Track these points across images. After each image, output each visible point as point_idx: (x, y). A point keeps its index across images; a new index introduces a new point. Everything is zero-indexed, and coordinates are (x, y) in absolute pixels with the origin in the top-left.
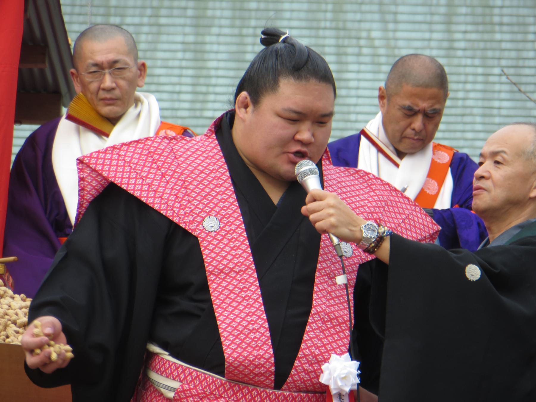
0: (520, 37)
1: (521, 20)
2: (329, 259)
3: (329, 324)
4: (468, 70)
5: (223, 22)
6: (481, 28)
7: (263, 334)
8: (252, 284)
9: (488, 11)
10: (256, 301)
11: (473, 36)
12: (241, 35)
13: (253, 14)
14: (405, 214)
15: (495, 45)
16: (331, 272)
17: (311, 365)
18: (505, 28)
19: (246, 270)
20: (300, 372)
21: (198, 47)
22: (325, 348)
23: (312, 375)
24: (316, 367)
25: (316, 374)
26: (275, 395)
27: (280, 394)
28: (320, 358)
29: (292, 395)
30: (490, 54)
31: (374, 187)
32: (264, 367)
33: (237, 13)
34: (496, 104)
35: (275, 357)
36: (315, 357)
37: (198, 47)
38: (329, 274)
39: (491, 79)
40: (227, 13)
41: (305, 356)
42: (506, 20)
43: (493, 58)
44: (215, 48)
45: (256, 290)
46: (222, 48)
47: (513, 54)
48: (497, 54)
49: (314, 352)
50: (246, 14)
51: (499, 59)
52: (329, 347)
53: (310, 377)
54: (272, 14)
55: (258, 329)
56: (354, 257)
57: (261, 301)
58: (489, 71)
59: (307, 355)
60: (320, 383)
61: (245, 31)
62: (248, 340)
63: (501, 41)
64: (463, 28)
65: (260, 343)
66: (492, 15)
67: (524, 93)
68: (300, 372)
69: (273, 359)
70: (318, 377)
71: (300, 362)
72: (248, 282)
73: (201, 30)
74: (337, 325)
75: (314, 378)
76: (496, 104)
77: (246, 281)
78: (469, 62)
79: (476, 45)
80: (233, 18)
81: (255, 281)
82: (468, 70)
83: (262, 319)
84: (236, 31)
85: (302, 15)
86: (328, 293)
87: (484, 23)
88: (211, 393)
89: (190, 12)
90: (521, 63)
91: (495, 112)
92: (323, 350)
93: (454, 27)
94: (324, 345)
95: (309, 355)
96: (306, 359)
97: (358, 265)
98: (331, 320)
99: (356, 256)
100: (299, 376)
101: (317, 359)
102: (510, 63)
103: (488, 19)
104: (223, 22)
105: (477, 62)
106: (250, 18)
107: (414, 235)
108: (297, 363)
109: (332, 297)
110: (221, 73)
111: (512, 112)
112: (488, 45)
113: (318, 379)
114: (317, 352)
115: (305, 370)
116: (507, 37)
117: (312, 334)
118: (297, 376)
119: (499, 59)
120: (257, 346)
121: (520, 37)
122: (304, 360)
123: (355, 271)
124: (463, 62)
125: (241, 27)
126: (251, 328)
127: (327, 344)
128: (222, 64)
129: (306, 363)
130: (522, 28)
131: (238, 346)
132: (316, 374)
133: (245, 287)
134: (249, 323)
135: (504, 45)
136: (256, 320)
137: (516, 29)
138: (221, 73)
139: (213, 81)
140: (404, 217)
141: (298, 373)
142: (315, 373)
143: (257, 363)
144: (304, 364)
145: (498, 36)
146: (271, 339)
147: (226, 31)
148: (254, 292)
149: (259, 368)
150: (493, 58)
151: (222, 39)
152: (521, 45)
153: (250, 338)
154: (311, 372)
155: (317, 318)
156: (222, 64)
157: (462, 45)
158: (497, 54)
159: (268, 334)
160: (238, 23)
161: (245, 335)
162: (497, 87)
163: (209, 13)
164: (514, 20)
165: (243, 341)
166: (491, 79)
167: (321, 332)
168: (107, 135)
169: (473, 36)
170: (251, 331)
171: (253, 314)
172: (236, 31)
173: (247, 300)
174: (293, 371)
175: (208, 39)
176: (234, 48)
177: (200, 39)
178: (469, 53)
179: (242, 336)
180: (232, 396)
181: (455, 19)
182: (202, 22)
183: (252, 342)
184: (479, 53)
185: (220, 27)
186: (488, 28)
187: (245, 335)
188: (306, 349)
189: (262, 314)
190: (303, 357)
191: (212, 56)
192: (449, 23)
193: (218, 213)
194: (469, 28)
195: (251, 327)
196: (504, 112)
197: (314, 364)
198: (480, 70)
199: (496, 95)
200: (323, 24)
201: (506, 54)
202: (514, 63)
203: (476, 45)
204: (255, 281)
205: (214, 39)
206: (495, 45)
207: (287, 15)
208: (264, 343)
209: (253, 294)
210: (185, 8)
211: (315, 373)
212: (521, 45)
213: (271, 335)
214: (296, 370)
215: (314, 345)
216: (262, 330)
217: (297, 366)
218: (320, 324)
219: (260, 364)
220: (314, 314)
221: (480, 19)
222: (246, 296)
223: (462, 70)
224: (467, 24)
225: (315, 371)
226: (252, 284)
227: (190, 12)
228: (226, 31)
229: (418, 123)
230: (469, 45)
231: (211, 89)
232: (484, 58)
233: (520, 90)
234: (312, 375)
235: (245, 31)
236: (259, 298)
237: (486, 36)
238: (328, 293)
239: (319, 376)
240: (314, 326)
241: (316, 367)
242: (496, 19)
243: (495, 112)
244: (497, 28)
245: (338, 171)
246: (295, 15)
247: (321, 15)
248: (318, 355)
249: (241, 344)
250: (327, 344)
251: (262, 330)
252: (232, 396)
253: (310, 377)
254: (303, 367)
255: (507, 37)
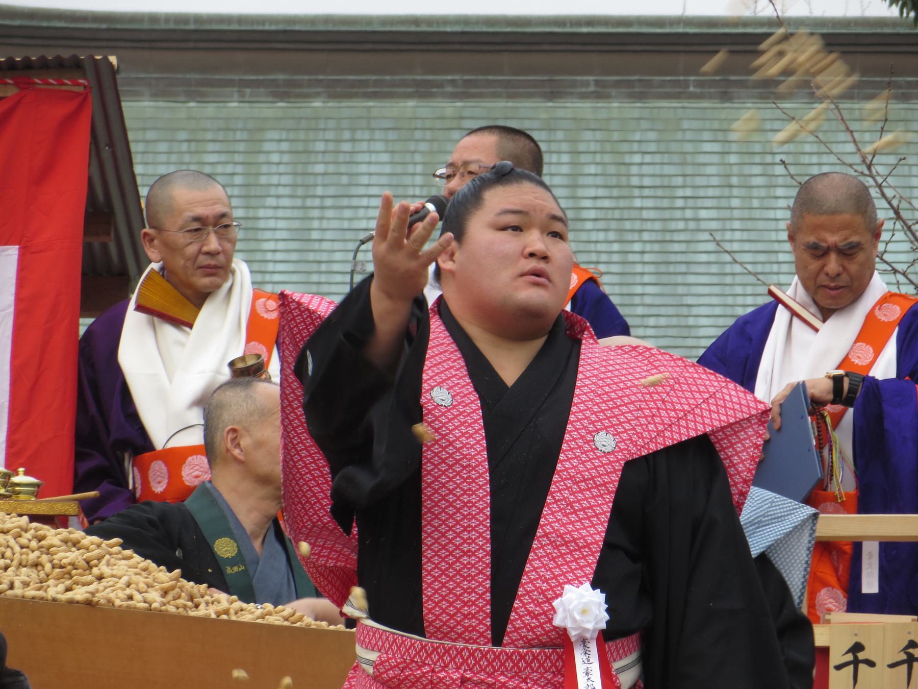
0: (665, 203)
1: (666, 181)
2: (577, 457)
3: (563, 550)
4: (600, 247)
5: (281, 191)
6: (615, 192)
7: (480, 560)
8: (481, 487)
9: (623, 169)
10: (481, 511)
11: (607, 203)
12: (304, 207)
13: (319, 180)
14: (708, 392)
15: (634, 214)
16: (577, 473)
17: (539, 605)
18: (646, 192)
19: (477, 466)
20: (523, 616)
21: (250, 224)
22: (557, 580)
23: (543, 619)
24: (546, 607)
25: (548, 618)
26: (494, 653)
27: (501, 652)
28: (550, 594)
29: (519, 653)
30: (628, 225)
31: (657, 364)
32: (476, 605)
33: (299, 180)
34: (639, 290)
35: (491, 593)
36: (543, 592)
37: (250, 224)
38: (574, 476)
39: (632, 258)
40: (286, 180)
41: (528, 593)
42: (647, 181)
43: (632, 231)
44: (272, 224)
45: (484, 496)
46: (281, 224)
47: (658, 226)
48: (637, 225)
49: (540, 587)
50: (310, 180)
51: (641, 231)
52: (561, 579)
53: (539, 622)
54: (345, 180)
55: (475, 551)
56: (618, 452)
57: (488, 513)
58: (627, 247)
59: (531, 592)
60: (555, 628)
61: (309, 202)
62: (458, 566)
63: (641, 209)
64: (592, 192)
65: (473, 572)
66: (629, 175)
67: (741, 264)
68: (523, 616)
69: (488, 594)
70: (550, 620)
71: (521, 601)
72: (476, 483)
73: (253, 202)
74: (575, 550)
75: (546, 623)
76: (639, 290)
77: (474, 481)
78: (601, 236)
79: (610, 214)
80: (294, 185)
81: (486, 484)
82: (600, 247)
83: (484, 538)
84: (299, 202)
85: (384, 180)
86: (568, 505)
87: (618, 186)
88: (412, 661)
89: (238, 180)
90: (668, 237)
91: (637, 300)
92: (553, 583)
93: (581, 192)
94: (555, 577)
95: (534, 591)
96: (530, 596)
97: (622, 462)
98: (566, 544)
99: (621, 450)
100: (522, 621)
101: (545, 596)
102: (654, 236)
103: (624, 180)
104: (281, 191)
105: (612, 236)
106: (316, 185)
107: (723, 418)
108: (517, 604)
109: (578, 510)
110: (279, 256)
111: (658, 301)
112: (626, 214)
113: (551, 624)
114: (545, 586)
115: (529, 613)
116: (649, 203)
117: (537, 564)
118: (519, 622)
119: (641, 231)
120: (469, 575)
121: (665, 203)
122: (526, 599)
123: (618, 470)
124: (594, 236)
125: (305, 197)
126: (465, 549)
127: (560, 575)
128: (281, 245)
129: (530, 603)
130: (667, 193)
131: (443, 572)
132: (548, 618)
133: (470, 489)
134: (465, 541)
135: (645, 214)
136: (476, 539)
137: (660, 192)
138: (279, 256)
139: (270, 267)
140: (706, 396)
141: (521, 617)
142: (546, 615)
143: (466, 599)
144: (527, 604)
145: (638, 203)
146: (491, 568)
147: (285, 202)
148: (481, 499)
149: (469, 607)
150: (632, 231)
151: (280, 213)
152: (667, 214)
153: (462, 564)
154: (540, 614)
155: (545, 541)
156: (281, 245)
157: (592, 214)
158: (637, 225)
159: (488, 560)
160: (300, 191)
161: (455, 557)
162: (639, 268)
163: (263, 180)
164: (658, 181)
165: (451, 566)
166: (632, 258)
167: (550, 560)
168: (191, 326)
169: (607, 203)
170: (465, 553)
171: (473, 529)
172: (299, 202)
173: (470, 508)
174: (513, 615)
175: (261, 213)
176: (296, 224)
177: (251, 213)
178: (601, 225)
179: (451, 559)
180: (438, 661)
181: (582, 181)
182: (253, 191)
183: (463, 568)
184: (613, 225)
185: (278, 197)
186: (625, 192)
187: (455, 557)
188: (529, 583)
189: (486, 531)
190: (525, 595)
191: (268, 235)
192: (575, 186)
193: (618, 434)
194: (601, 192)
195: (465, 547)
196: (648, 300)
197: (542, 603)
198: (616, 247)
199: (638, 279)
200: (410, 192)
201: (649, 225)
202: (659, 237)
203: (610, 214)
204: (486, 484)
205: (270, 213)
206: (634, 214)
207: (364, 180)
208: (481, 572)
209: (479, 501)
210: (233, 174)
211: (546, 615)
212: (667, 214)
213: (492, 562)
214: (517, 613)
215: (540, 577)
216: (481, 554)
217: (518, 608)
218: (549, 549)
219: (470, 601)
220: (540, 537)
221: (613, 181)
222: (469, 502)
223: (592, 247)
224: (597, 187)
225: (545, 613)
226: (481, 487)
227: (238, 180)
228: (285, 202)
229: (833, 264)
230: (600, 214)
231: (268, 278)
232: (621, 231)
233: (735, 261)
234: (543, 619)
235: (309, 202)
236: (486, 507)
237: (622, 203)
238: (568, 505)
239: (552, 619)
240: (541, 552)
241: (546, 607)
242: (635, 181)
243: (637, 300)
244: (636, 192)
245: (295, 404)
246: (374, 180)
247: (407, 180)
248: (547, 590)
249: (447, 569)
250: (560, 575)
251: (481, 554)
252: (438, 661)
253: (539, 622)
254: (526, 608)
255: (649, 203)
